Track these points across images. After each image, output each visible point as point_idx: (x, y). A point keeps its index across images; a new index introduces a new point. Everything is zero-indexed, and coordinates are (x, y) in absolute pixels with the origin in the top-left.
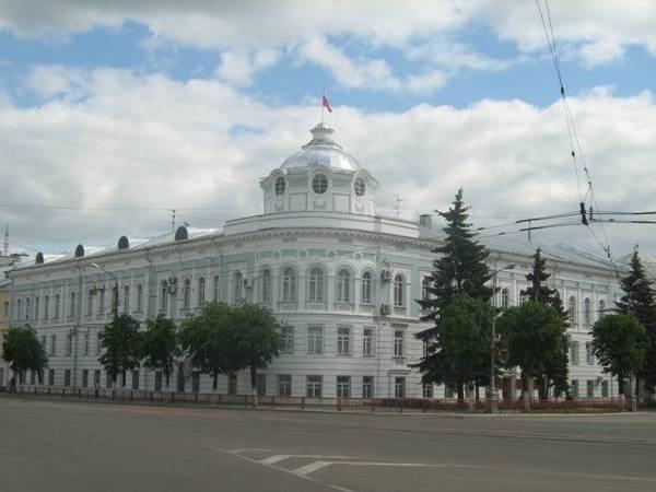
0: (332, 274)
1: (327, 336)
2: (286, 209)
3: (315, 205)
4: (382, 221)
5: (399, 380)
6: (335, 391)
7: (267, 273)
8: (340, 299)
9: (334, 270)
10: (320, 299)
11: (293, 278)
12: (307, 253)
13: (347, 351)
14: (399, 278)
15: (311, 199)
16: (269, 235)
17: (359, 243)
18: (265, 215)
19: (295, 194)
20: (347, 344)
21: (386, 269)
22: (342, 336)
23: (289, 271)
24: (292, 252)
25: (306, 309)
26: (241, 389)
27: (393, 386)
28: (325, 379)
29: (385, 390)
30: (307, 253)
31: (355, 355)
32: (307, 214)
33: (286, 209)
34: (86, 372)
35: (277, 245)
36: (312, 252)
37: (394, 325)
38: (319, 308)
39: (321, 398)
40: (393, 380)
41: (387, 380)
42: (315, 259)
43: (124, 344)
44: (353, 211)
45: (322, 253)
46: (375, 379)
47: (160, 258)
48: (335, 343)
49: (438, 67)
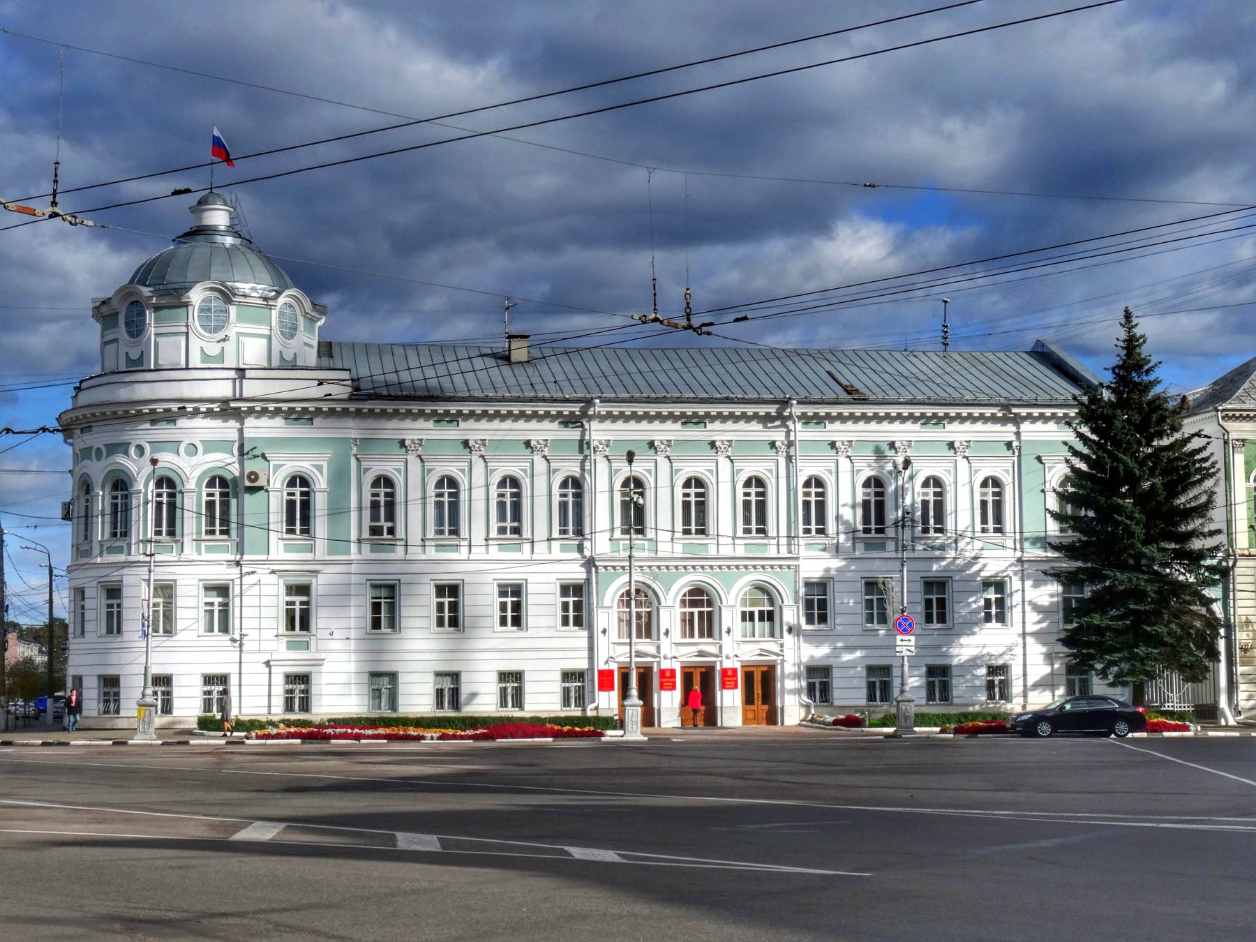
11: (126, 497)
15: (195, 344)
44: (586, 354)
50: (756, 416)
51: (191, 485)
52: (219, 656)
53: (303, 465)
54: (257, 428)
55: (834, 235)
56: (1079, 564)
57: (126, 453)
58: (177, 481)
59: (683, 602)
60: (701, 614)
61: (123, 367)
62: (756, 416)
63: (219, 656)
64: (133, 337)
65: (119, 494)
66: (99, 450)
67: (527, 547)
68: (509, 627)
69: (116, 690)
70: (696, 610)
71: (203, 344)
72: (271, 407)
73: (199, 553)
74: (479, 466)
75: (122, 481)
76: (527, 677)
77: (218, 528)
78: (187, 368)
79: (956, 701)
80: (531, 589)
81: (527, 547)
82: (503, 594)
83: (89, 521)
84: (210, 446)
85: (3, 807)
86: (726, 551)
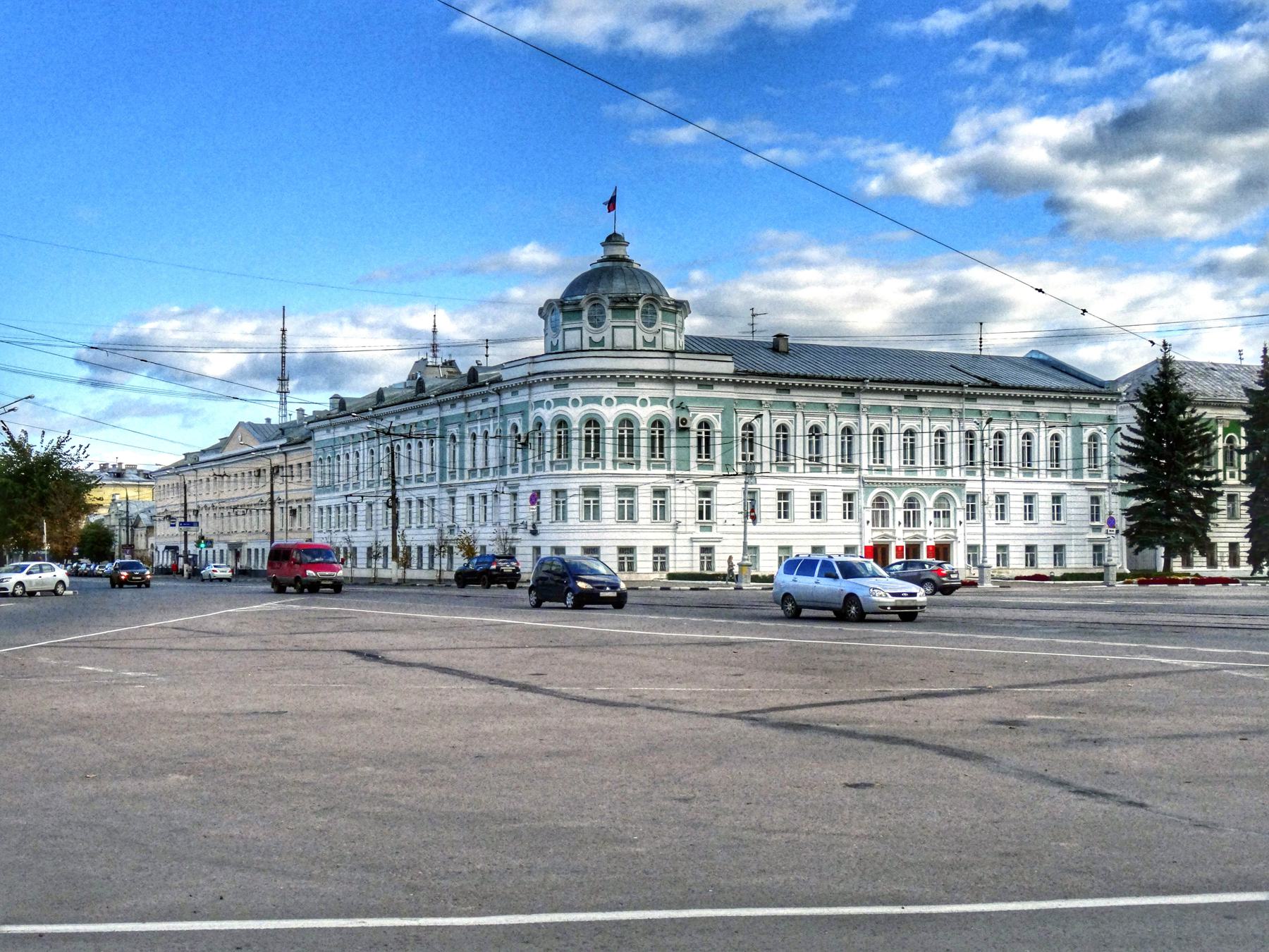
0: (643, 426)
1: (641, 500)
2: (608, 345)
3: (592, 342)
4: (677, 355)
5: (704, 550)
6: (651, 564)
7: (540, 424)
8: (653, 456)
9: (646, 420)
10: (596, 456)
12: (581, 401)
13: (631, 517)
14: (705, 424)
16: (545, 380)
17: (643, 385)
18: (547, 354)
19: (570, 329)
20: (663, 508)
21: (683, 415)
22: (658, 499)
23: (562, 423)
24: (632, 400)
25: (615, 469)
26: (1073, 561)
27: (697, 557)
28: (638, 551)
29: (1078, 559)
30: (615, 400)
31: (641, 521)
32: (584, 354)
33: (560, 349)
34: (420, 549)
35: (547, 393)
36: (587, 400)
37: (696, 483)
38: (596, 466)
39: (1065, 568)
40: (697, 550)
41: (688, 550)
42: (627, 408)
43: (753, 493)
45: (597, 400)
46: (671, 550)
47: (508, 395)
48: (650, 507)
49: (1146, 24)
50: (902, 392)
51: (576, 426)
52: (662, 536)
53: (709, 415)
54: (683, 391)
55: (1198, 277)
56: (1140, 486)
57: (567, 405)
58: (599, 421)
59: (905, 505)
60: (914, 512)
61: (586, 346)
62: (902, 392)
63: (662, 536)
64: (594, 326)
65: (562, 430)
66: (548, 402)
67: (1007, 474)
68: (847, 520)
69: (630, 555)
70: (911, 510)
71: (591, 335)
72: (694, 377)
73: (580, 469)
74: (832, 418)
75: (565, 422)
76: (761, 550)
77: (626, 452)
78: (635, 350)
79: (1040, 566)
80: (796, 495)
81: (792, 468)
82: (812, 499)
83: (665, 445)
84: (655, 401)
85: (1266, 598)
86: (926, 475)
